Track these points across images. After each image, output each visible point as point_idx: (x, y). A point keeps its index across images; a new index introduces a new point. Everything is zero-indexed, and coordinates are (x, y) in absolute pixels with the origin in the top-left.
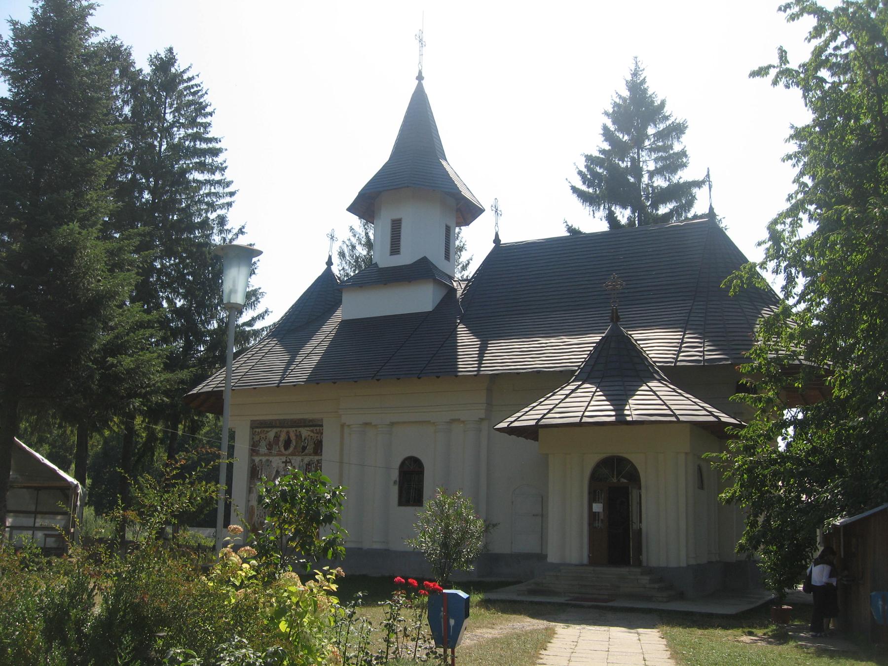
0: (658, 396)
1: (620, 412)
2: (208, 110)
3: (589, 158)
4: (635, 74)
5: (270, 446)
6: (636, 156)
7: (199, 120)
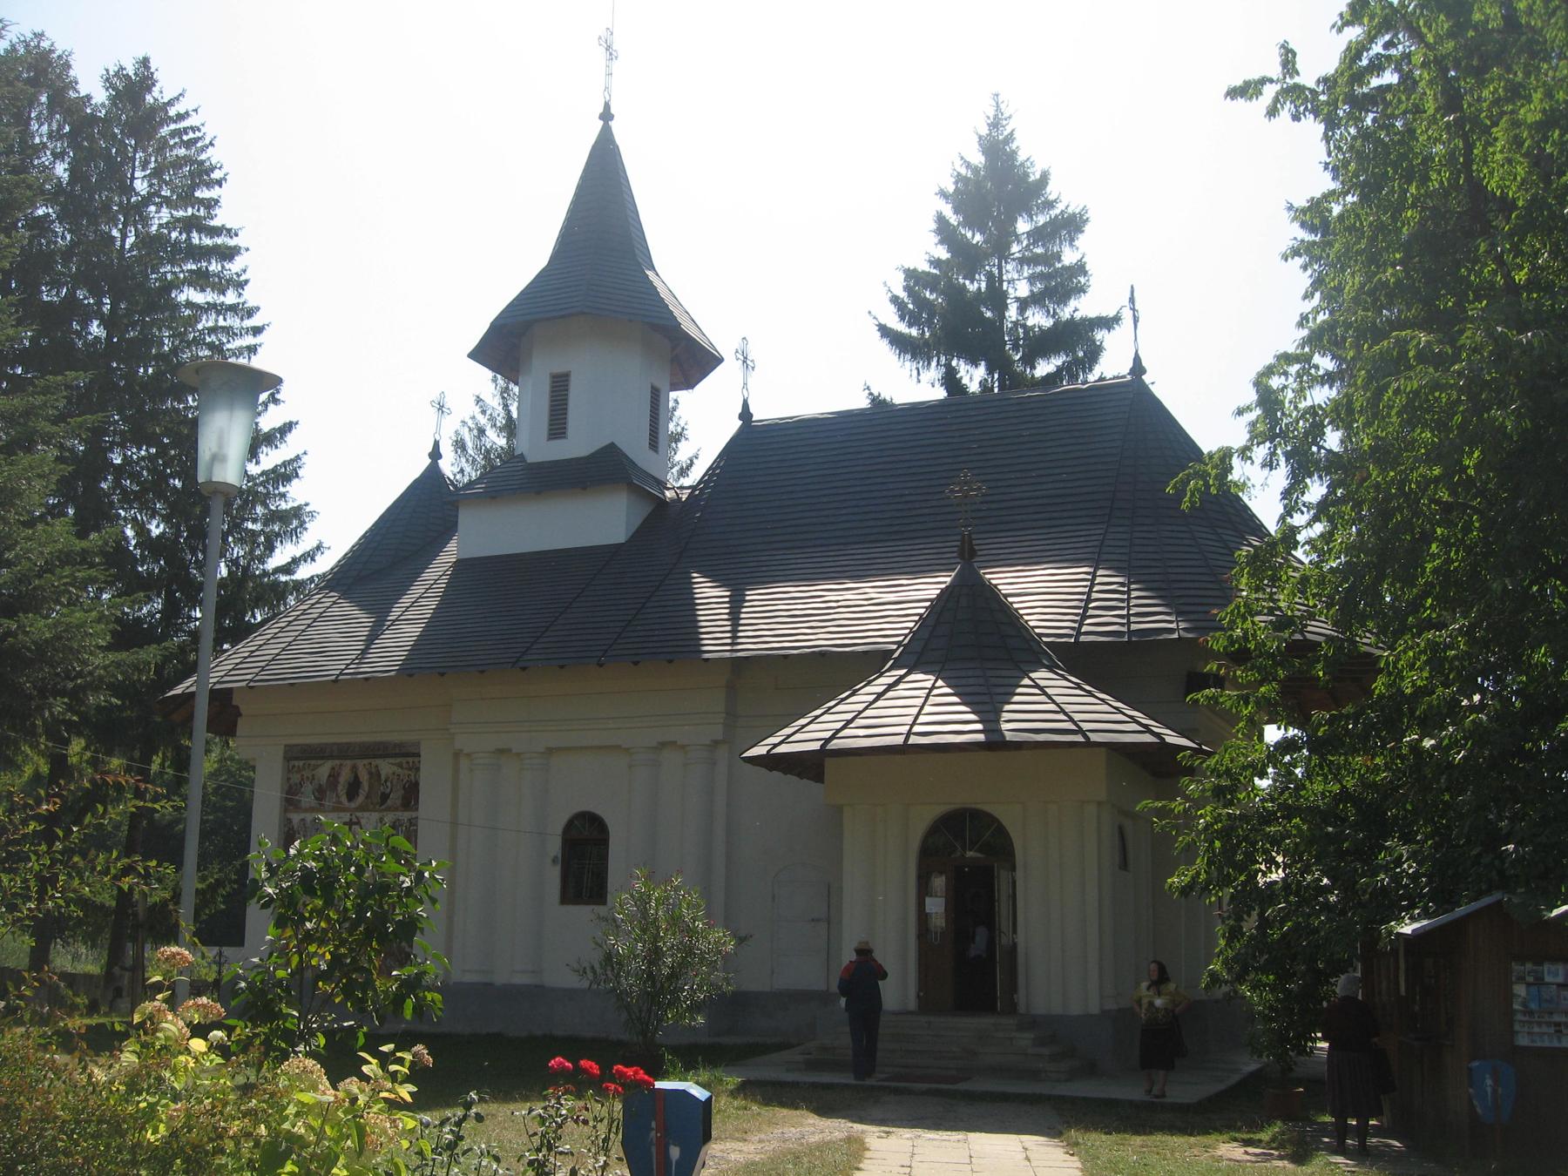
0: (1049, 697)
1: (992, 726)
2: (216, 175)
3: (911, 274)
4: (995, 124)
5: (320, 793)
6: (995, 271)
7: (198, 194)
